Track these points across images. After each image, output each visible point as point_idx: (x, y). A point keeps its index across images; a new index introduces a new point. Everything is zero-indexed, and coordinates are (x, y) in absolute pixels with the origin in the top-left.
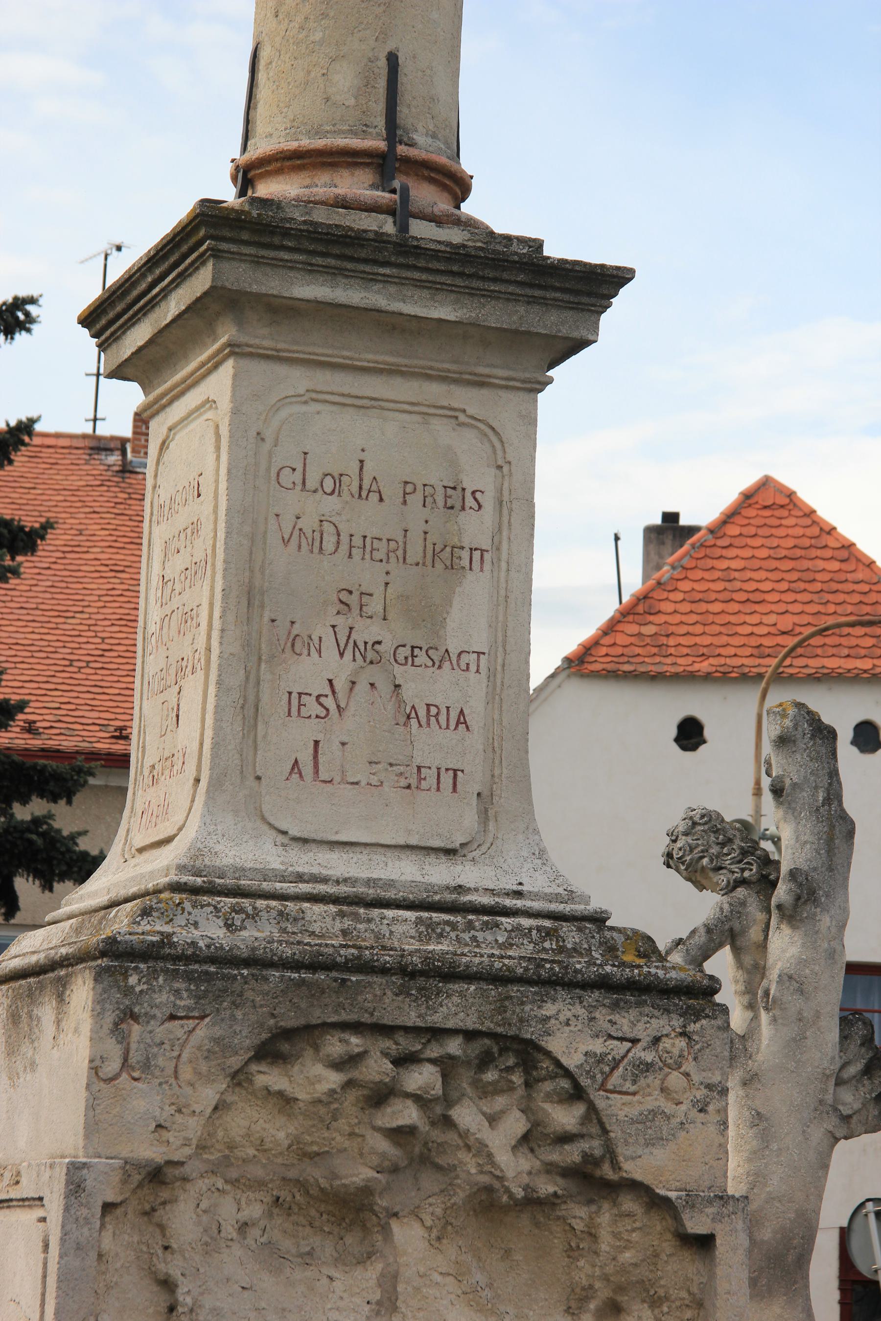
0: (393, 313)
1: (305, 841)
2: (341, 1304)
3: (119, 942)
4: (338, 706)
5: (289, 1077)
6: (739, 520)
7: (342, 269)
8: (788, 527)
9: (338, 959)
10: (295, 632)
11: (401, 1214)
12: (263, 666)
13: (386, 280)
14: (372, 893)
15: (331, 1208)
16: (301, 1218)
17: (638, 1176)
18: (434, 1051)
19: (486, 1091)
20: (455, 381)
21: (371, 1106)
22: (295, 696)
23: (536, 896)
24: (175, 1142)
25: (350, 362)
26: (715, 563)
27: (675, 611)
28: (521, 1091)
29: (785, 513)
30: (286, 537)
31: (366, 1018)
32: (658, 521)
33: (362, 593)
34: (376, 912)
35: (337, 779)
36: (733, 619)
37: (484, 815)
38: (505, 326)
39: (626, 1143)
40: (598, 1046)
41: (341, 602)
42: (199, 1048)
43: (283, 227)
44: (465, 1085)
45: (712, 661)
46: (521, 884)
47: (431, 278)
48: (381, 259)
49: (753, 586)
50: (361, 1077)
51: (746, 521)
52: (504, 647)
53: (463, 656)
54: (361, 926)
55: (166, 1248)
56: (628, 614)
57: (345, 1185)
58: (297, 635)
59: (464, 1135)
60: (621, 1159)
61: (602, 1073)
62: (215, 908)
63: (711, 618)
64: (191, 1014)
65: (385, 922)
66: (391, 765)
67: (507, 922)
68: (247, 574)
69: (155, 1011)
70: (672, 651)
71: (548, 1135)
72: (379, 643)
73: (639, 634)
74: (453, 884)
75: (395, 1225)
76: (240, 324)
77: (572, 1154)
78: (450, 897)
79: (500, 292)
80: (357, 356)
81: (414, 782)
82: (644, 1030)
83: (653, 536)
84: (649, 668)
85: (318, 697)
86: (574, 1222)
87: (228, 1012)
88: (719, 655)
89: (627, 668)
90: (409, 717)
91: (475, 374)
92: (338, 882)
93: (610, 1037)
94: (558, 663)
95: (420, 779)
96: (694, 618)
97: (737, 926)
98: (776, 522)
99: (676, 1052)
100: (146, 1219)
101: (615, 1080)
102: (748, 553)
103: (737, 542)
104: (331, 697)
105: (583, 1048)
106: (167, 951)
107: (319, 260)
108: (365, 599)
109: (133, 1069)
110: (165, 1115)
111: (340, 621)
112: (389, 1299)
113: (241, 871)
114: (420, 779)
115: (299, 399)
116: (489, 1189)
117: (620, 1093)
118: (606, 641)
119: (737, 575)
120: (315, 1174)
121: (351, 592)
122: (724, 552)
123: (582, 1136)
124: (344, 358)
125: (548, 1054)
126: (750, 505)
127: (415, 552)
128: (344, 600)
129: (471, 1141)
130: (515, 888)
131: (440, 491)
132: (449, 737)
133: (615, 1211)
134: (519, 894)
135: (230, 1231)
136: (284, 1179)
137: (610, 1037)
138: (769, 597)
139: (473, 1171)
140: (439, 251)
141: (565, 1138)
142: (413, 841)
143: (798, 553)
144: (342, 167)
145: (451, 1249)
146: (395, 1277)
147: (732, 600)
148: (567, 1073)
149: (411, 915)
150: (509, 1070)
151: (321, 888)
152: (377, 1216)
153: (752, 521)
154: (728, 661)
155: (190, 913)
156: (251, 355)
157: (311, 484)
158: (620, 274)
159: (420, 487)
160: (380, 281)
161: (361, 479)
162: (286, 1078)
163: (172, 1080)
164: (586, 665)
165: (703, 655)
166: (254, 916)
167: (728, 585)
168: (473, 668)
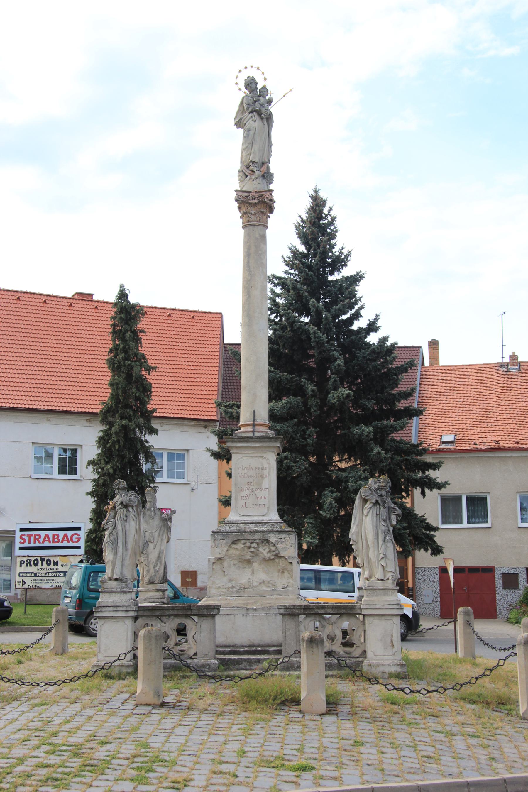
19: (264, 546)
37: (268, 510)
40: (276, 539)
77: (274, 553)
113: (233, 520)
120: (243, 557)
127: (258, 476)
135: (232, 565)
141: (274, 551)
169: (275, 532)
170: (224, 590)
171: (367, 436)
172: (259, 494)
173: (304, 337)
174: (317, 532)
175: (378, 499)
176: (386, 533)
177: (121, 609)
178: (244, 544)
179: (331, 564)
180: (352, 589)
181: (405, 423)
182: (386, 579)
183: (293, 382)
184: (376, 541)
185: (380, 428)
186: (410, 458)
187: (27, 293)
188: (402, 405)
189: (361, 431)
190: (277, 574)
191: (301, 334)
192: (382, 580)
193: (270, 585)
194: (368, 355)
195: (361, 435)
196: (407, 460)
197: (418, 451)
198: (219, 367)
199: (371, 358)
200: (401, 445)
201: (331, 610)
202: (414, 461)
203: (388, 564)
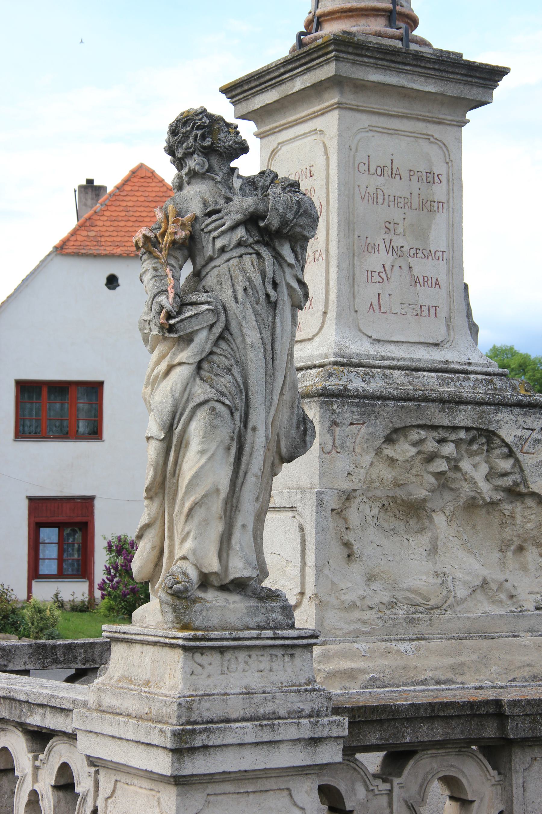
0: (410, 88)
1: (379, 341)
2: (415, 551)
3: (328, 390)
4: (387, 277)
5: (394, 450)
6: (130, 183)
7: (389, 67)
8: (152, 187)
9: (415, 396)
10: (368, 242)
11: (436, 511)
12: (356, 258)
13: (407, 72)
14: (414, 365)
15: (404, 508)
16: (391, 514)
17: (536, 490)
18: (454, 437)
19: (471, 454)
20: (429, 122)
21: (425, 463)
22: (369, 272)
23: (477, 365)
24: (356, 481)
25: (387, 112)
26: (121, 203)
27: (104, 225)
28: (485, 454)
29: (150, 180)
30: (363, 196)
31: (428, 423)
32: (84, 183)
33: (394, 223)
34: (420, 374)
35: (388, 311)
36: (130, 229)
38: (455, 95)
39: (531, 476)
40: (519, 433)
41: (386, 227)
42: (363, 438)
43: (367, 46)
44: (463, 452)
45: (121, 248)
46: (469, 359)
47: (426, 72)
48: (406, 62)
49: (138, 214)
50: (424, 449)
51: (133, 184)
52: (453, 250)
53: (437, 253)
54: (416, 380)
55: (347, 529)
56: (82, 226)
57: (415, 498)
58: (369, 244)
59: (464, 475)
60: (529, 483)
61: (521, 445)
62: (357, 373)
63: (120, 229)
64: (359, 422)
65: (425, 378)
66: (409, 304)
67: (472, 376)
68: (348, 214)
69: (345, 421)
70: (103, 244)
71: (497, 473)
72: (402, 247)
73: (88, 236)
74: (443, 360)
75: (434, 515)
76: (342, 93)
77: (508, 482)
78: (445, 366)
79: (454, 79)
80: (390, 109)
81: (419, 312)
83: (83, 190)
84: (93, 252)
85: (379, 273)
86: (505, 512)
87: (374, 421)
88: (125, 246)
89: (83, 251)
90: (416, 282)
91: (439, 118)
92: (398, 360)
93: (524, 428)
94: (51, 249)
95: (422, 311)
96: (112, 229)
98: (147, 185)
100: (338, 515)
101: (526, 448)
102: (135, 199)
103: (130, 193)
104: (384, 273)
105: (514, 434)
106: (347, 393)
107: (380, 62)
108: (396, 226)
109: (337, 448)
110: (351, 469)
111: (386, 236)
112: (434, 548)
114: (422, 311)
115: (365, 130)
116: (474, 498)
117: (528, 453)
118: (73, 239)
119: (130, 209)
120: (401, 493)
121: (390, 223)
122: (124, 198)
123: (511, 473)
124: (385, 110)
125: (499, 437)
126: (135, 177)
127: (415, 204)
128: (387, 226)
129: (467, 477)
130: (468, 361)
131: (424, 174)
133: (523, 506)
136: (388, 496)
137: (524, 428)
138: (146, 219)
139: (467, 490)
140: (431, 58)
141: (505, 474)
142: (422, 341)
143: (158, 199)
144: (371, 16)
147: (129, 220)
148: (507, 445)
149: (433, 374)
150: (483, 444)
151: (394, 363)
152: (426, 511)
153: (136, 184)
154: (129, 248)
155: (347, 376)
156: (346, 108)
157: (372, 171)
158: (505, 70)
159: (416, 173)
160: (404, 73)
161: (392, 169)
162: (393, 451)
163: (353, 453)
164: (64, 250)
165: (117, 245)
166: (373, 376)
167: (127, 213)
168: (441, 258)
170: (368, 615)
177: (292, 733)
190: (497, 555)
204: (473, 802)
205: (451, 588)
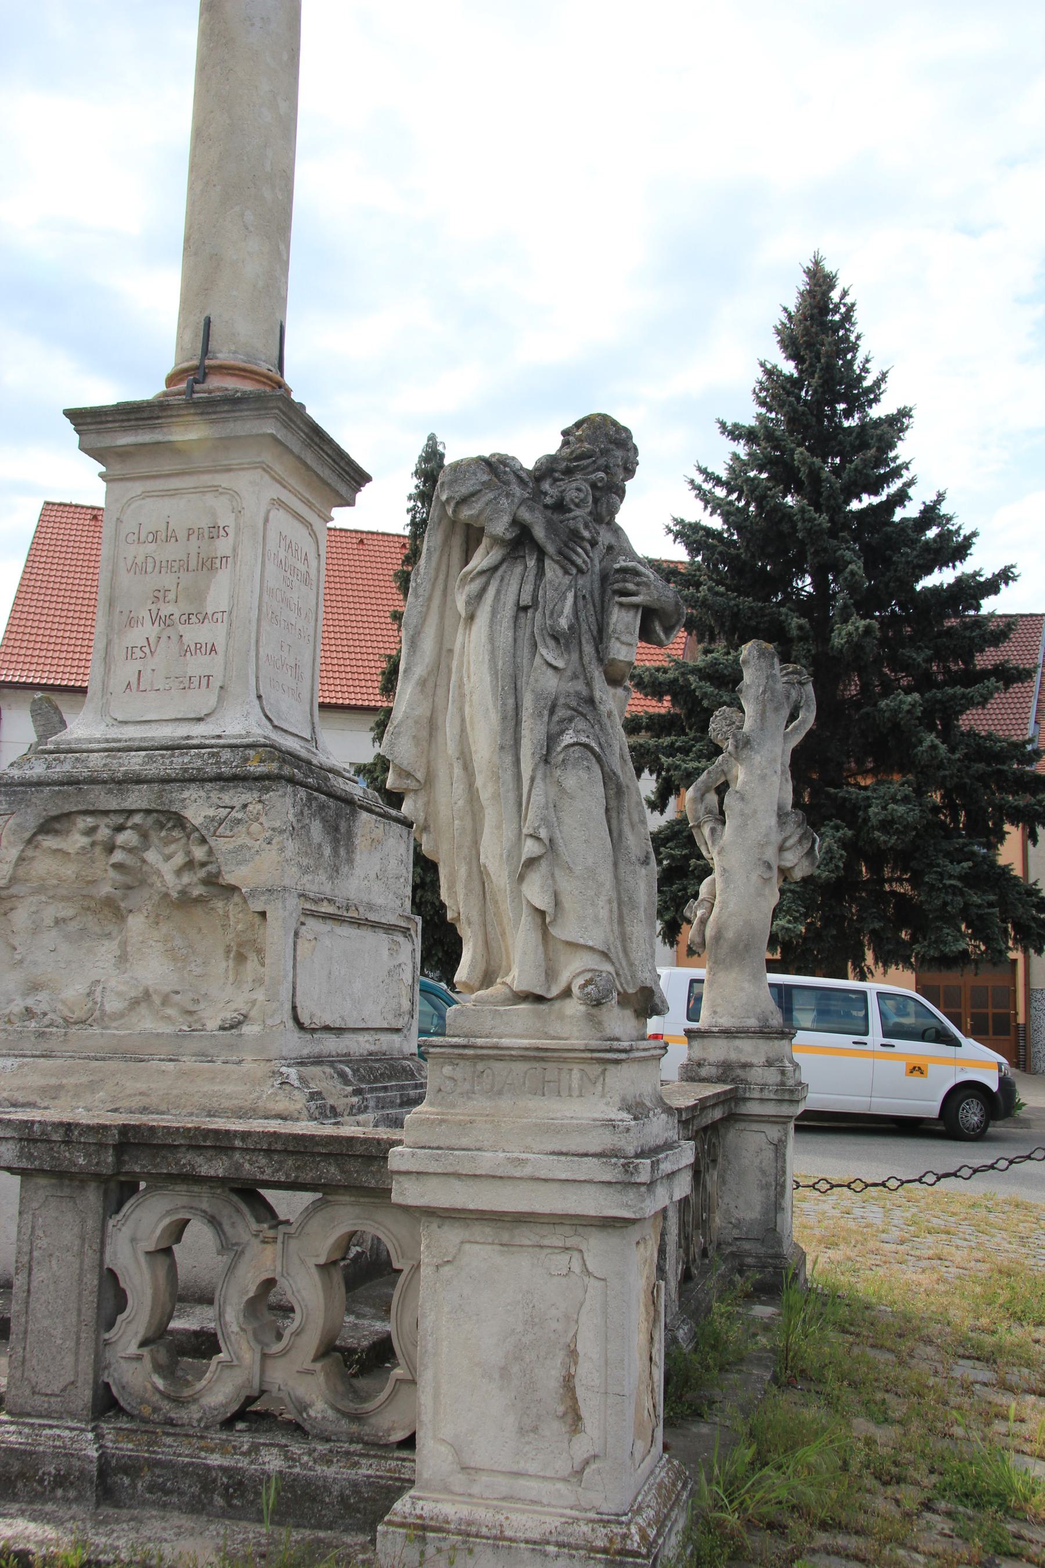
19: (167, 842)
20: (216, 471)
31: (91, 808)
37: (220, 699)
40: (211, 812)
82: (237, 802)
97: (726, 768)
99: (255, 812)
101: (221, 830)
105: (203, 814)
107: (126, 424)
111: (153, 607)
127: (193, 564)
131: (206, 530)
132: (203, 659)
134: (219, 737)
135: (49, 921)
141: (203, 865)
142: (179, 716)
145: (164, 928)
146: (125, 943)
157: (142, 540)
159: (196, 530)
168: (220, 620)
169: (211, 780)
171: (909, 712)
172: (194, 633)
173: (785, 527)
174: (802, 910)
175: (525, 515)
176: (561, 713)
178: (91, 831)
179: (845, 977)
180: (862, 1028)
181: (991, 687)
182: (555, 992)
183: (763, 616)
184: (509, 759)
185: (940, 702)
186: (1005, 768)
187: (377, 534)
188: (986, 659)
189: (897, 702)
191: (780, 521)
192: (539, 999)
193: (169, 1011)
194: (916, 557)
195: (896, 711)
196: (1000, 771)
197: (1023, 755)
198: (685, 644)
199: (921, 562)
200: (988, 744)
201: (263, 1161)
202: (1014, 773)
203: (567, 902)
204: (400, 1271)
205: (99, 1000)
